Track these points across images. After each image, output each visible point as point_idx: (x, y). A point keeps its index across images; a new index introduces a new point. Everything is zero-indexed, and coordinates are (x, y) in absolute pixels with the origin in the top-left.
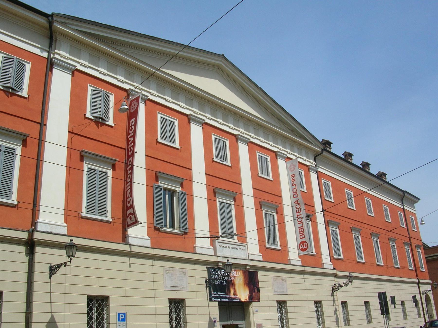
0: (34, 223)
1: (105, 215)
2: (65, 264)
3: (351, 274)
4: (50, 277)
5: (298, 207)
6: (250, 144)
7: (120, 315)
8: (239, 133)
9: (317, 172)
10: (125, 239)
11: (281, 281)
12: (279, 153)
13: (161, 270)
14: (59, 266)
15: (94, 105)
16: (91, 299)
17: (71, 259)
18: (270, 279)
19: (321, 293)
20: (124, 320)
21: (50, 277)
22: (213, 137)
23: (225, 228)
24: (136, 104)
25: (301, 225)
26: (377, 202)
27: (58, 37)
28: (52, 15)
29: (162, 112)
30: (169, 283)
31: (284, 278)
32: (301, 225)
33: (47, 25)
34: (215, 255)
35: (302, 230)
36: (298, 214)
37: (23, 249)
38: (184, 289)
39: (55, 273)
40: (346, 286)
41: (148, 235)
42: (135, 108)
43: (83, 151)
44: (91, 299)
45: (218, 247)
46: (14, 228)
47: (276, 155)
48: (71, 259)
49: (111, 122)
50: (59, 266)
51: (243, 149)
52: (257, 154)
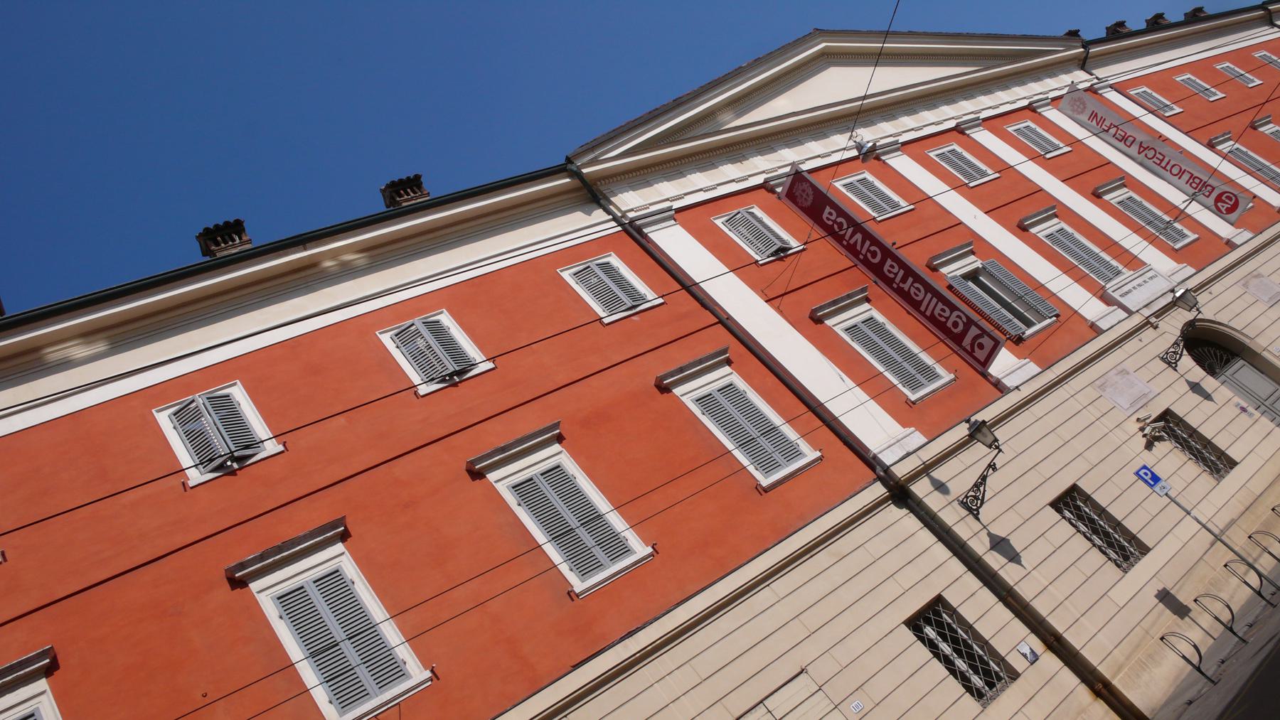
0: (870, 461)
1: (799, 454)
2: (992, 466)
3: (973, 419)
4: (978, 519)
5: (1151, 154)
6: (681, 214)
7: (1141, 473)
8: (765, 176)
9: (1111, 86)
10: (1000, 388)
11: (1255, 281)
12: (638, 223)
13: (1092, 393)
14: (983, 478)
15: (418, 358)
16: (915, 623)
17: (997, 447)
18: (1238, 290)
19: (1047, 469)
20: (1156, 479)
21: (978, 519)
22: (719, 222)
23: (1096, 264)
24: (805, 186)
25: (1186, 177)
26: (1241, 57)
27: (603, 188)
28: (569, 160)
29: (718, 213)
30: (1124, 401)
31: (1119, 368)
32: (1186, 177)
33: (577, 183)
34: (1130, 313)
35: (1197, 181)
36: (1163, 164)
37: (893, 512)
38: (1151, 396)
39: (982, 503)
40: (992, 466)
41: (904, 426)
42: (810, 192)
43: (472, 463)
44: (915, 623)
45: (1122, 300)
46: (858, 489)
47: (1034, 110)
48: (997, 447)
49: (794, 244)
50: (983, 478)
51: (984, 137)
52: (932, 155)
